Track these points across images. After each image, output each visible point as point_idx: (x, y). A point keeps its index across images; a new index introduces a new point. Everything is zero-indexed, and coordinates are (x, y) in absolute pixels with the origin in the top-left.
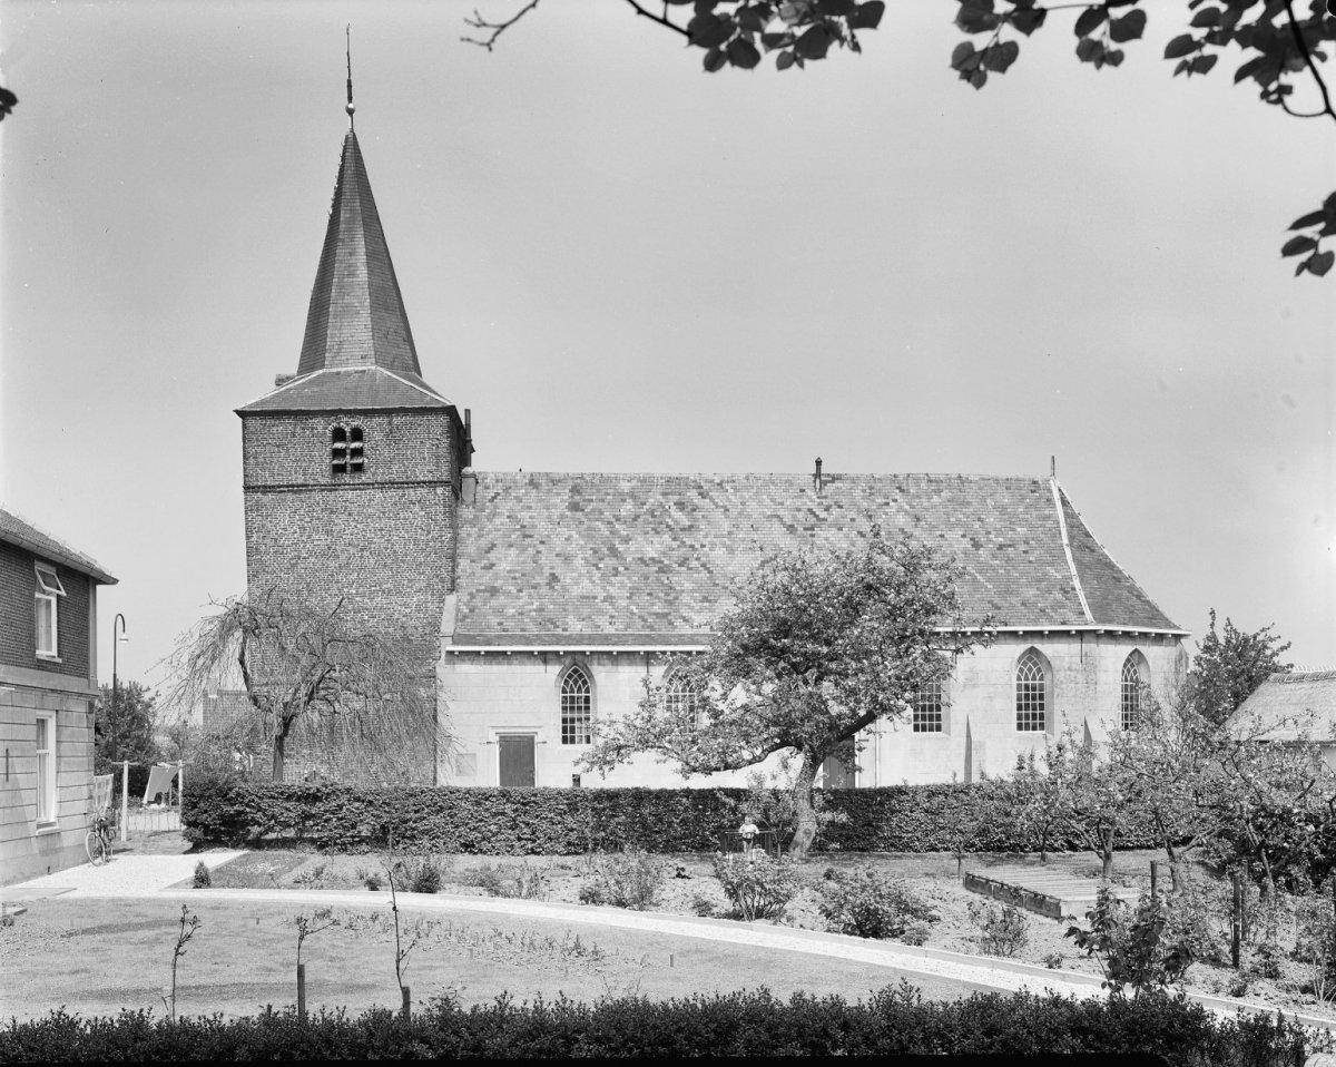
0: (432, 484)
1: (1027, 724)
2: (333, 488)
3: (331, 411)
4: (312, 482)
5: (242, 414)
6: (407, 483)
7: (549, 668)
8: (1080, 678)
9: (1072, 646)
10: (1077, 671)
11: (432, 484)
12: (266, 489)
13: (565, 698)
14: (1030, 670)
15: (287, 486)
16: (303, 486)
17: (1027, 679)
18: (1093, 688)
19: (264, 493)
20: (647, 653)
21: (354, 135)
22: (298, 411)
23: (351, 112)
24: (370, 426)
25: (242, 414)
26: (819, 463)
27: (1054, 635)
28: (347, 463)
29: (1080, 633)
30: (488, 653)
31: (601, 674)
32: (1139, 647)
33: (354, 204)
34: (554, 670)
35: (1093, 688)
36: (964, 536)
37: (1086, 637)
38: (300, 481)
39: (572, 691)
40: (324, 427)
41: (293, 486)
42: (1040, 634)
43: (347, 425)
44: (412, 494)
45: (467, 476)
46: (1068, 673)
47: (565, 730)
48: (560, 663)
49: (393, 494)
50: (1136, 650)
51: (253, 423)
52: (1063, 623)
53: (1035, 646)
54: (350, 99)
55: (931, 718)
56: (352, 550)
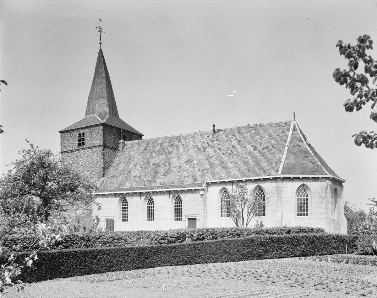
0: (99, 146)
2: (78, 150)
3: (77, 129)
4: (74, 149)
5: (61, 132)
6: (93, 147)
7: (117, 198)
8: (276, 196)
9: (273, 183)
10: (274, 193)
11: (99, 146)
12: (65, 152)
13: (148, 207)
15: (69, 151)
16: (72, 150)
17: (301, 196)
19: (64, 153)
20: (140, 193)
21: (101, 50)
22: (71, 130)
23: (100, 43)
24: (86, 131)
25: (61, 132)
26: (214, 126)
27: (265, 180)
28: (81, 142)
29: (275, 179)
30: (103, 195)
31: (129, 199)
33: (102, 70)
34: (118, 199)
36: (252, 146)
38: (71, 149)
40: (76, 133)
41: (70, 151)
42: (259, 180)
43: (81, 132)
44: (94, 150)
45: (120, 143)
46: (271, 194)
48: (119, 197)
49: (91, 150)
50: (304, 185)
51: (63, 134)
52: (268, 175)
53: (259, 184)
54: (100, 40)
55: (304, 211)
56: (82, 167)
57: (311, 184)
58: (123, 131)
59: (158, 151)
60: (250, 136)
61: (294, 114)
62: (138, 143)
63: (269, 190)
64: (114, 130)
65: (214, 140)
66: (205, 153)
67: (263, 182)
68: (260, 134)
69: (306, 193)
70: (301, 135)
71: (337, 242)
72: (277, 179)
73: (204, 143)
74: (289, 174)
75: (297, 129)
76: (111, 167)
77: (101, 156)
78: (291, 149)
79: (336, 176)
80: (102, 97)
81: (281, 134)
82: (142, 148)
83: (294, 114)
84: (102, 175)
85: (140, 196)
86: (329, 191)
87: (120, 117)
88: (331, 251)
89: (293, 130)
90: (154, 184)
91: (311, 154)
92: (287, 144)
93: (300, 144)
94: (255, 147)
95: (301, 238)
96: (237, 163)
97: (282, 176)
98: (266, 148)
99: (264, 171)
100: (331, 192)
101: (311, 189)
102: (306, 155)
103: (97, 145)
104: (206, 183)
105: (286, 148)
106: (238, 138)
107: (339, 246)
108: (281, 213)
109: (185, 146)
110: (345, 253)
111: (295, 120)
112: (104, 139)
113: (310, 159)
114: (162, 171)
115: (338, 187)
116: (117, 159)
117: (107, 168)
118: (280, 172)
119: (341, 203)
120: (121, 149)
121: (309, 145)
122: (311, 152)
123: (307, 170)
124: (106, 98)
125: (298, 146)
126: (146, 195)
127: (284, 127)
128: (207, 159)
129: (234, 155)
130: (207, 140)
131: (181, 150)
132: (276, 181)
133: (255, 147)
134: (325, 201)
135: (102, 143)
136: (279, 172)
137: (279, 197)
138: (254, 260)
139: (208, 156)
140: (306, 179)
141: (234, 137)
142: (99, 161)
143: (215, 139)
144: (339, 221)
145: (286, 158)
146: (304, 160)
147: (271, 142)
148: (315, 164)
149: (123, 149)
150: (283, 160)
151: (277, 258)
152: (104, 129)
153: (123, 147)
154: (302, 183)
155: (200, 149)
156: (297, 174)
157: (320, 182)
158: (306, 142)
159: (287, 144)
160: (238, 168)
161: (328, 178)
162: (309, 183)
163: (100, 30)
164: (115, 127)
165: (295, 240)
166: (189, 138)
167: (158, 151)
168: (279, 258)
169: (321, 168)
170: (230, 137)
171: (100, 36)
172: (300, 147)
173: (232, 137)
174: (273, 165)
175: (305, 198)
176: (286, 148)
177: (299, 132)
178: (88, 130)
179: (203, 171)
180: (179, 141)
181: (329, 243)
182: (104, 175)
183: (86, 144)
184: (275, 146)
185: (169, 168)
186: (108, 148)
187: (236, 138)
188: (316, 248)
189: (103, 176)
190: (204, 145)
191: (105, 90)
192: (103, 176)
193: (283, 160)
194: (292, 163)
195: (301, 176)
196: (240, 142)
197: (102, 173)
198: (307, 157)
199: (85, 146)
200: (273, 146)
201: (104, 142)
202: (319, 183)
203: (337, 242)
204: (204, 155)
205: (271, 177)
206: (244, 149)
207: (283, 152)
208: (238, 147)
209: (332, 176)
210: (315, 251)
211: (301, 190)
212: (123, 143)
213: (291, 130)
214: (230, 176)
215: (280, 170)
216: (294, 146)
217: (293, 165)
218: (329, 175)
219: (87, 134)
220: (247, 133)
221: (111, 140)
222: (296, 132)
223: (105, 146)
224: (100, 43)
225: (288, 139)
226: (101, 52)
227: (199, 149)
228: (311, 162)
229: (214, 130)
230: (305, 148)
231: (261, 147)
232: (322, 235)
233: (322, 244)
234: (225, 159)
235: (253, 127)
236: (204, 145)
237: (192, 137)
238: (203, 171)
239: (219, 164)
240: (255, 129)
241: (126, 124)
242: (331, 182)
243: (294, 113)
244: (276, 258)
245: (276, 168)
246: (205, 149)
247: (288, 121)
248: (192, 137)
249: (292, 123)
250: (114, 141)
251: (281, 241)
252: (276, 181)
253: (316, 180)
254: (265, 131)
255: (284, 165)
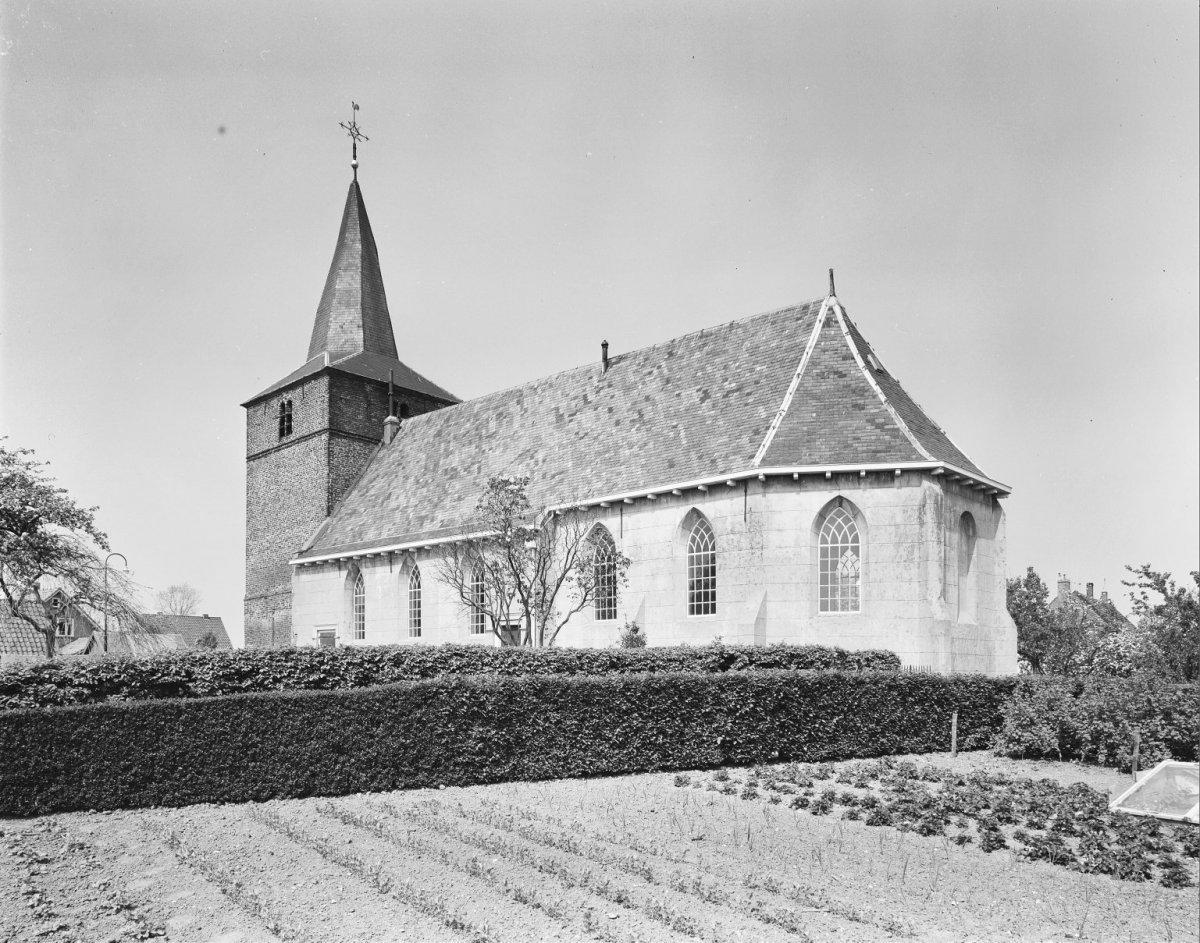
0: (319, 433)
1: (834, 603)
2: (278, 449)
8: (745, 543)
9: (735, 500)
10: (740, 533)
11: (319, 433)
14: (702, 538)
17: (834, 540)
18: (758, 553)
23: (355, 167)
24: (293, 395)
25: (247, 405)
26: (605, 346)
27: (715, 488)
29: (743, 484)
32: (699, 507)
35: (758, 553)
37: (752, 487)
39: (699, 550)
47: (824, 593)
48: (346, 568)
49: (303, 444)
50: (840, 500)
52: (722, 473)
54: (355, 157)
57: (863, 496)
58: (394, 391)
59: (464, 436)
60: (699, 360)
61: (832, 276)
62: (428, 421)
63: (724, 523)
64: (368, 388)
65: (602, 388)
66: (571, 425)
67: (707, 497)
68: (725, 352)
69: (852, 529)
70: (849, 340)
71: (914, 704)
72: (749, 484)
73: (575, 398)
74: (787, 463)
75: (837, 322)
76: (354, 488)
77: (324, 459)
78: (809, 384)
79: (983, 476)
80: (348, 305)
81: (786, 343)
82: (433, 431)
83: (832, 276)
84: (325, 513)
85: (391, 562)
86: (930, 517)
87: (402, 358)
88: (884, 740)
89: (823, 327)
90: (428, 527)
91: (875, 396)
92: (800, 369)
93: (842, 367)
94: (705, 392)
95: (712, 689)
96: (646, 444)
97: (762, 472)
98: (737, 390)
99: (713, 461)
100: (939, 523)
101: (867, 514)
102: (859, 402)
103: (316, 430)
104: (550, 512)
105: (795, 383)
106: (666, 371)
107: (924, 723)
108: (760, 600)
109: (529, 412)
110: (944, 748)
111: (834, 295)
112: (330, 413)
113: (872, 411)
114: (458, 487)
115: (979, 511)
116: (374, 466)
117: (343, 492)
118: (757, 460)
119: (996, 567)
120: (386, 439)
121: (880, 374)
122: (877, 389)
123: (856, 449)
124: (359, 307)
125: (835, 373)
126: (404, 558)
127: (798, 319)
128: (573, 443)
129: (644, 423)
130: (584, 390)
131: (516, 425)
132: (746, 492)
133: (705, 392)
134: (916, 554)
135: (326, 425)
136: (753, 460)
137: (754, 545)
138: (437, 787)
139: (577, 433)
140: (847, 480)
141: (656, 371)
142: (320, 473)
143: (606, 383)
144: (986, 629)
145: (790, 414)
146: (849, 416)
147: (752, 370)
148: (886, 427)
149: (391, 440)
150: (776, 422)
151: (574, 777)
152: (331, 386)
153: (395, 435)
154: (835, 494)
155: (562, 415)
156: (818, 463)
157: (900, 487)
158: (868, 363)
159: (800, 369)
160: (643, 461)
161: (926, 473)
162: (861, 491)
163: (354, 131)
164: (370, 381)
165: (682, 699)
166: (543, 391)
167: (464, 436)
168: (585, 775)
169: (907, 440)
170: (646, 371)
171: (355, 148)
172: (842, 375)
173: (650, 373)
174: (745, 440)
175: (827, 548)
176: (795, 383)
177: (844, 329)
178: (299, 390)
179: (553, 477)
180: (518, 403)
181: (873, 707)
182: (329, 511)
183: (294, 430)
184: (763, 381)
185: (475, 478)
186: (345, 437)
187: (661, 373)
188: (799, 731)
189: (329, 514)
190: (573, 403)
191: (359, 286)
192: (329, 514)
193: (776, 422)
194: (805, 429)
195: (828, 469)
196: (668, 381)
197: (324, 504)
198: (861, 407)
199: (292, 437)
200: (757, 382)
201: (331, 421)
202: (894, 490)
203: (914, 704)
204: (568, 432)
205: (727, 477)
206: (675, 401)
207: (783, 397)
208: (659, 397)
209: (942, 464)
210: (793, 742)
211: (832, 521)
212: (392, 423)
213: (818, 327)
214: (615, 485)
215: (761, 454)
216: (822, 375)
217: (809, 433)
218: (931, 462)
219: (296, 403)
220: (692, 352)
221: (356, 416)
222: (833, 333)
223: (334, 431)
224: (355, 167)
225: (805, 354)
226: (355, 191)
227: (560, 417)
228: (871, 421)
229: (607, 361)
230: (858, 378)
231: (721, 388)
232: (835, 676)
233: (833, 715)
234: (618, 435)
235: (712, 334)
236: (573, 403)
237: (551, 386)
238: (553, 477)
239: (599, 454)
240: (715, 341)
241: (414, 376)
242: (937, 488)
243: (831, 271)
244: (570, 776)
245: (749, 450)
246: (575, 414)
247: (808, 298)
248: (551, 386)
249: (823, 304)
250: (369, 418)
251: (598, 702)
252: (746, 492)
253: (885, 482)
254: (743, 341)
255: (776, 435)
